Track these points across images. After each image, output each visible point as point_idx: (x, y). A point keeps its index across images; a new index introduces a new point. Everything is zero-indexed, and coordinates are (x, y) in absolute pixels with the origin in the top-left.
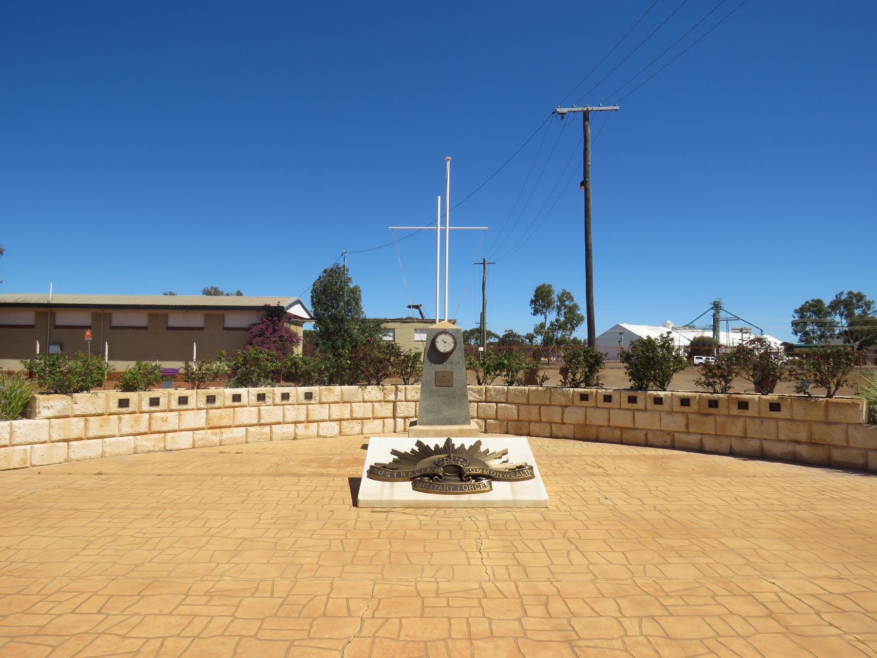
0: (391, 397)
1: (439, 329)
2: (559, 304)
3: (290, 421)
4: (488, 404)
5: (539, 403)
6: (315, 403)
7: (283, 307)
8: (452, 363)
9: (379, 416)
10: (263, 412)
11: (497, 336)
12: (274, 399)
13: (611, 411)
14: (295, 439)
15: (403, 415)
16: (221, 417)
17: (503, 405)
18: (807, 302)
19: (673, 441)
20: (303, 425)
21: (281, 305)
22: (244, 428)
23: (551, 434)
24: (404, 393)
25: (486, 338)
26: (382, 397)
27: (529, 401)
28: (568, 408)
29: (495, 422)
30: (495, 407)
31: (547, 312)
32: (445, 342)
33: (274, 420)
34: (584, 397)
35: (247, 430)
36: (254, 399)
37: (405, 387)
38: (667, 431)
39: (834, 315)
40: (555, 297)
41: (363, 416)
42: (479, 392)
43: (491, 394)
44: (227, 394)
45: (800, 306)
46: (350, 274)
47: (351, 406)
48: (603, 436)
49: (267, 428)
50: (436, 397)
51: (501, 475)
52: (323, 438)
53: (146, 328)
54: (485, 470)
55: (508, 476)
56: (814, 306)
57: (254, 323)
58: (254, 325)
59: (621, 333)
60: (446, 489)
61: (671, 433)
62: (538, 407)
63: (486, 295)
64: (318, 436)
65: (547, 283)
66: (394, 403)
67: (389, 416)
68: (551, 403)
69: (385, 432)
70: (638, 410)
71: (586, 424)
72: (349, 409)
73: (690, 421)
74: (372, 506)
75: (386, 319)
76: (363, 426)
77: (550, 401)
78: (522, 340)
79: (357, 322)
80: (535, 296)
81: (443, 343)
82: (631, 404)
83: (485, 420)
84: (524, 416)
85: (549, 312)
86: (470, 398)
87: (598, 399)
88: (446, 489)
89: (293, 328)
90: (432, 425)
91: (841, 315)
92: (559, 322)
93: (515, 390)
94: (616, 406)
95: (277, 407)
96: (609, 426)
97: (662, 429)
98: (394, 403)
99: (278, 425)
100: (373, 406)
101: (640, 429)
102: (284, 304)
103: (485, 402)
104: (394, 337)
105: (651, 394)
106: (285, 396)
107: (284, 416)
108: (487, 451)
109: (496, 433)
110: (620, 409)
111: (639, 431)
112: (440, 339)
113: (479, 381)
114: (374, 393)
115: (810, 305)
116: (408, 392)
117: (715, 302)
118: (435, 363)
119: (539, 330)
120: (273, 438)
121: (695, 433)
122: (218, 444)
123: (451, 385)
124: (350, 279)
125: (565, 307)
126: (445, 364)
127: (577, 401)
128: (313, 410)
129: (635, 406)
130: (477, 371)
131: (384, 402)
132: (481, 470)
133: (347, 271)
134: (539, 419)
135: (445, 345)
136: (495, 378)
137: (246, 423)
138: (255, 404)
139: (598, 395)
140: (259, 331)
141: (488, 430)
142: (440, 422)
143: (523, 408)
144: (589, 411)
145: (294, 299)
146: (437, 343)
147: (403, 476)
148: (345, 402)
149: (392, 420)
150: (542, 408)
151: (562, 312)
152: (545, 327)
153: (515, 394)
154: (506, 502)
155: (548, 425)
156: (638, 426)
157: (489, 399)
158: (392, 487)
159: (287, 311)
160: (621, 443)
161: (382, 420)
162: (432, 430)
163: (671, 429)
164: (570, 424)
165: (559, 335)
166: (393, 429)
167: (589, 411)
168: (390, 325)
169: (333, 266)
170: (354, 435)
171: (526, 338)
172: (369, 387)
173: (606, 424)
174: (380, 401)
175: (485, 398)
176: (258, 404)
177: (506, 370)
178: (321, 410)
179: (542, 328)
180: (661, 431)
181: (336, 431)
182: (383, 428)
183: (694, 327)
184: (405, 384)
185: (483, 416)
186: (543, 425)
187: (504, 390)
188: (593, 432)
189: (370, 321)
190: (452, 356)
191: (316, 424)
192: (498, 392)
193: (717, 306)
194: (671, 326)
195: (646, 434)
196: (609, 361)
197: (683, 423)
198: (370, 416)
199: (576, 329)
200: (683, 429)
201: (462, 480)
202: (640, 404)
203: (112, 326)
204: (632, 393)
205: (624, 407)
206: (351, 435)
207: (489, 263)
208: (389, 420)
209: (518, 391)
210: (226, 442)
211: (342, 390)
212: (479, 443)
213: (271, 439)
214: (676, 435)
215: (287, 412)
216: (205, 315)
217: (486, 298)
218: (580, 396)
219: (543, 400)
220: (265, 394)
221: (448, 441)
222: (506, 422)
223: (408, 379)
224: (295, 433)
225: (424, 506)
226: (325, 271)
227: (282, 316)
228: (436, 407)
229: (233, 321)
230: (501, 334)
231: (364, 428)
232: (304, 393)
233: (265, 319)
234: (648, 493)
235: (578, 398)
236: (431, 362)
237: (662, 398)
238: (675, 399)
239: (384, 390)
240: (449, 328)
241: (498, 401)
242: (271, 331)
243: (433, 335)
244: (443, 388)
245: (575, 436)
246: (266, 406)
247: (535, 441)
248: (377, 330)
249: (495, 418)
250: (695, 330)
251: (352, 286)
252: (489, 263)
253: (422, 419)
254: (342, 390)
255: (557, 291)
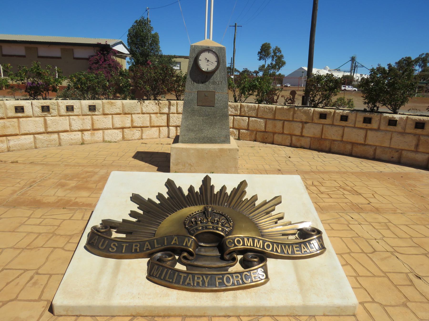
0: (165, 110)
1: (202, 46)
2: (273, 54)
3: (77, 129)
4: (242, 117)
5: (284, 119)
6: (99, 114)
7: (109, 45)
8: (214, 83)
9: (156, 125)
10: (49, 122)
11: (239, 72)
12: (59, 110)
13: (369, 132)
14: (82, 144)
15: (175, 124)
16: (4, 127)
17: (254, 119)
18: (403, 58)
19: (400, 157)
20: (89, 132)
21: (108, 43)
22: (32, 136)
23: (291, 143)
24: (175, 107)
25: (234, 71)
26: (158, 110)
27: (275, 116)
28: (308, 124)
29: (247, 132)
30: (247, 120)
31: (267, 59)
32: (208, 61)
33: (60, 129)
34: (323, 116)
35: (35, 138)
36: (38, 111)
37: (177, 102)
38: (396, 149)
39: (415, 66)
40: (271, 50)
41: (142, 125)
42: (235, 108)
43: (244, 110)
44: (8, 106)
45: (399, 60)
46: (152, 24)
47: (132, 117)
48: (335, 148)
49: (55, 136)
50: (197, 116)
51: (279, 251)
52: (108, 143)
53: (24, 56)
54: (256, 241)
55: (290, 252)
56: (406, 61)
57: (92, 55)
58: (92, 56)
59: (303, 72)
60: (198, 283)
61: (400, 151)
62: (282, 122)
63: (235, 46)
64: (104, 141)
65: (268, 42)
66: (168, 114)
67: (164, 125)
68: (293, 120)
69: (161, 137)
70: (371, 130)
71: (322, 138)
72: (130, 119)
73: (421, 142)
74: (78, 314)
75: (175, 56)
76: (142, 133)
77: (293, 117)
78: (252, 74)
79: (157, 57)
80: (261, 50)
81: (206, 61)
82: (365, 124)
83: (239, 130)
84: (270, 128)
85: (268, 59)
86: (230, 113)
87: (335, 118)
88: (198, 283)
89: (118, 60)
90: (193, 143)
91: (420, 66)
92: (272, 65)
93: (264, 108)
94: (351, 125)
95: (63, 117)
96: (342, 141)
97: (392, 146)
98: (168, 114)
99: (65, 133)
100: (151, 117)
101: (370, 145)
102: (111, 42)
103: (239, 116)
104: (180, 67)
105: (386, 117)
106: (70, 109)
107: (70, 125)
108: (255, 198)
109: (247, 140)
110: (355, 127)
111: (370, 147)
112: (203, 57)
113: (235, 99)
114: (151, 106)
115: (404, 60)
116: (179, 107)
117: (352, 57)
118: (198, 82)
119: (262, 68)
120: (62, 144)
121: (424, 153)
122: (6, 150)
123: (213, 106)
124: (152, 28)
125: (276, 56)
126: (207, 83)
127: (316, 120)
128: (98, 120)
129: (369, 126)
130: (234, 91)
131: (160, 114)
132: (251, 240)
133: (150, 22)
134: (282, 131)
135: (208, 64)
136: (248, 97)
137: (33, 131)
138: (40, 115)
139: (336, 115)
140: (96, 60)
141: (241, 138)
142: (201, 140)
143: (269, 122)
144: (325, 127)
145: (120, 40)
146: (199, 61)
147: (136, 250)
148: (126, 114)
149: (166, 128)
150: (286, 123)
151: (275, 59)
152: (265, 67)
153: (264, 111)
154: (293, 308)
155: (289, 136)
156: (368, 142)
157: (243, 114)
158: (117, 269)
159: (113, 48)
160: (351, 155)
161: (158, 128)
162: (193, 149)
163: (400, 147)
164: (308, 137)
165: (272, 72)
166: (167, 135)
167: (325, 127)
168: (178, 60)
169: (141, 18)
170: (135, 140)
171: (254, 73)
172: (147, 102)
173: (339, 138)
174: (156, 113)
175: (240, 113)
176: (43, 115)
177: (257, 90)
178: (105, 120)
179: (263, 68)
180: (390, 148)
181: (120, 136)
182: (159, 134)
183: (340, 70)
184: (178, 100)
185: (237, 127)
186: (285, 136)
187: (255, 107)
188: (327, 144)
189: (165, 56)
190: (214, 76)
191: (101, 132)
192: (250, 109)
193: (353, 59)
194: (328, 69)
195: (375, 150)
196: (295, 87)
197: (414, 142)
198: (148, 125)
199: (281, 69)
200: (413, 148)
201: (222, 258)
202: (374, 125)
203: (3, 54)
204: (368, 115)
205: (359, 126)
206: (132, 140)
207: (238, 26)
208: (164, 128)
209: (267, 108)
210: (14, 148)
211: (123, 104)
212: (243, 184)
213: (60, 145)
214: (404, 153)
215: (73, 122)
216: (61, 49)
217: (235, 48)
218: (319, 115)
219: (287, 116)
220: (49, 106)
221: (206, 180)
222: (255, 132)
223: (180, 96)
224: (83, 139)
225: (162, 314)
226: (136, 22)
227: (110, 51)
228: (197, 126)
229: (79, 53)
230: (241, 70)
231: (144, 134)
232: (88, 106)
233: (99, 53)
234: (312, 158)
235: (318, 116)
236: (194, 81)
237: (396, 121)
238: (409, 122)
239: (159, 104)
240: (213, 46)
241: (250, 115)
242: (103, 61)
243: (196, 52)
244: (204, 107)
245: (311, 147)
246: (52, 116)
247: (280, 150)
248: (169, 63)
249: (247, 128)
250: (340, 72)
251: (153, 33)
252: (238, 26)
253: (184, 137)
254: (123, 104)
255: (273, 47)
